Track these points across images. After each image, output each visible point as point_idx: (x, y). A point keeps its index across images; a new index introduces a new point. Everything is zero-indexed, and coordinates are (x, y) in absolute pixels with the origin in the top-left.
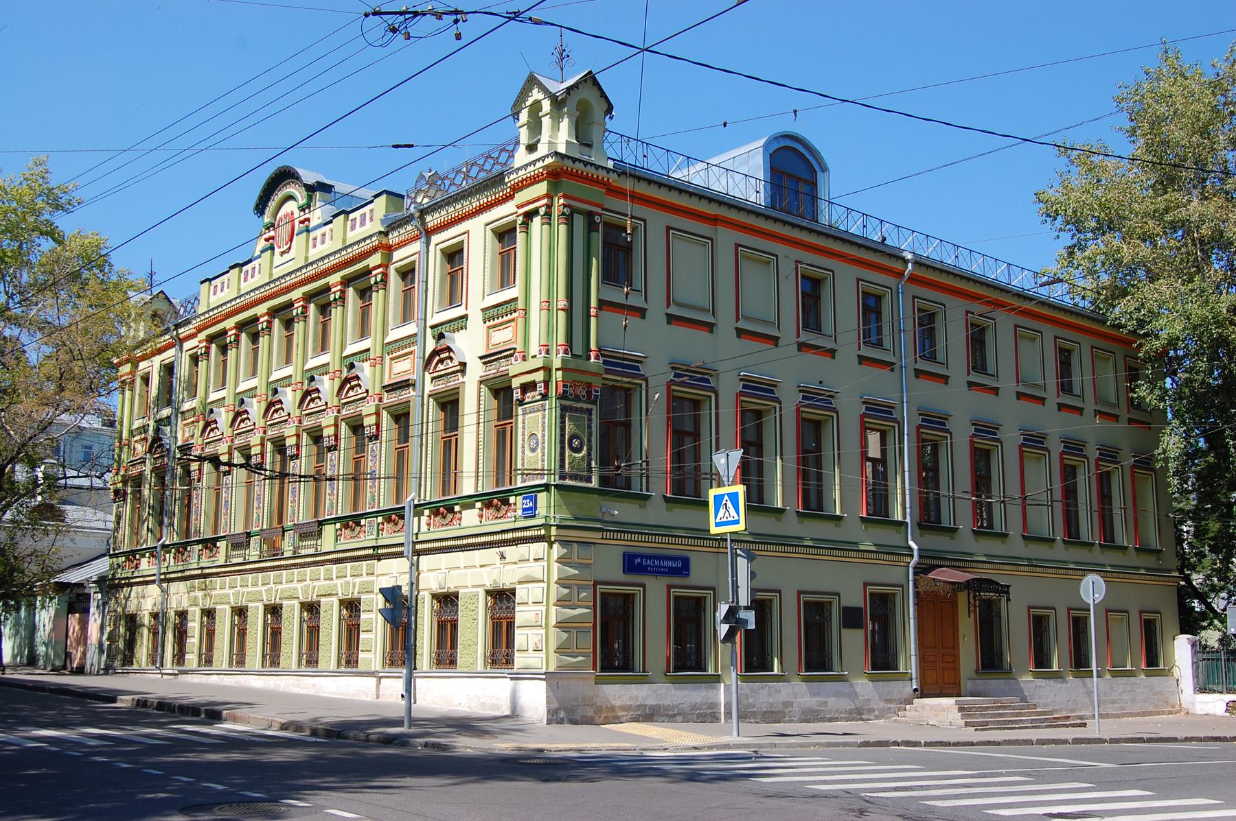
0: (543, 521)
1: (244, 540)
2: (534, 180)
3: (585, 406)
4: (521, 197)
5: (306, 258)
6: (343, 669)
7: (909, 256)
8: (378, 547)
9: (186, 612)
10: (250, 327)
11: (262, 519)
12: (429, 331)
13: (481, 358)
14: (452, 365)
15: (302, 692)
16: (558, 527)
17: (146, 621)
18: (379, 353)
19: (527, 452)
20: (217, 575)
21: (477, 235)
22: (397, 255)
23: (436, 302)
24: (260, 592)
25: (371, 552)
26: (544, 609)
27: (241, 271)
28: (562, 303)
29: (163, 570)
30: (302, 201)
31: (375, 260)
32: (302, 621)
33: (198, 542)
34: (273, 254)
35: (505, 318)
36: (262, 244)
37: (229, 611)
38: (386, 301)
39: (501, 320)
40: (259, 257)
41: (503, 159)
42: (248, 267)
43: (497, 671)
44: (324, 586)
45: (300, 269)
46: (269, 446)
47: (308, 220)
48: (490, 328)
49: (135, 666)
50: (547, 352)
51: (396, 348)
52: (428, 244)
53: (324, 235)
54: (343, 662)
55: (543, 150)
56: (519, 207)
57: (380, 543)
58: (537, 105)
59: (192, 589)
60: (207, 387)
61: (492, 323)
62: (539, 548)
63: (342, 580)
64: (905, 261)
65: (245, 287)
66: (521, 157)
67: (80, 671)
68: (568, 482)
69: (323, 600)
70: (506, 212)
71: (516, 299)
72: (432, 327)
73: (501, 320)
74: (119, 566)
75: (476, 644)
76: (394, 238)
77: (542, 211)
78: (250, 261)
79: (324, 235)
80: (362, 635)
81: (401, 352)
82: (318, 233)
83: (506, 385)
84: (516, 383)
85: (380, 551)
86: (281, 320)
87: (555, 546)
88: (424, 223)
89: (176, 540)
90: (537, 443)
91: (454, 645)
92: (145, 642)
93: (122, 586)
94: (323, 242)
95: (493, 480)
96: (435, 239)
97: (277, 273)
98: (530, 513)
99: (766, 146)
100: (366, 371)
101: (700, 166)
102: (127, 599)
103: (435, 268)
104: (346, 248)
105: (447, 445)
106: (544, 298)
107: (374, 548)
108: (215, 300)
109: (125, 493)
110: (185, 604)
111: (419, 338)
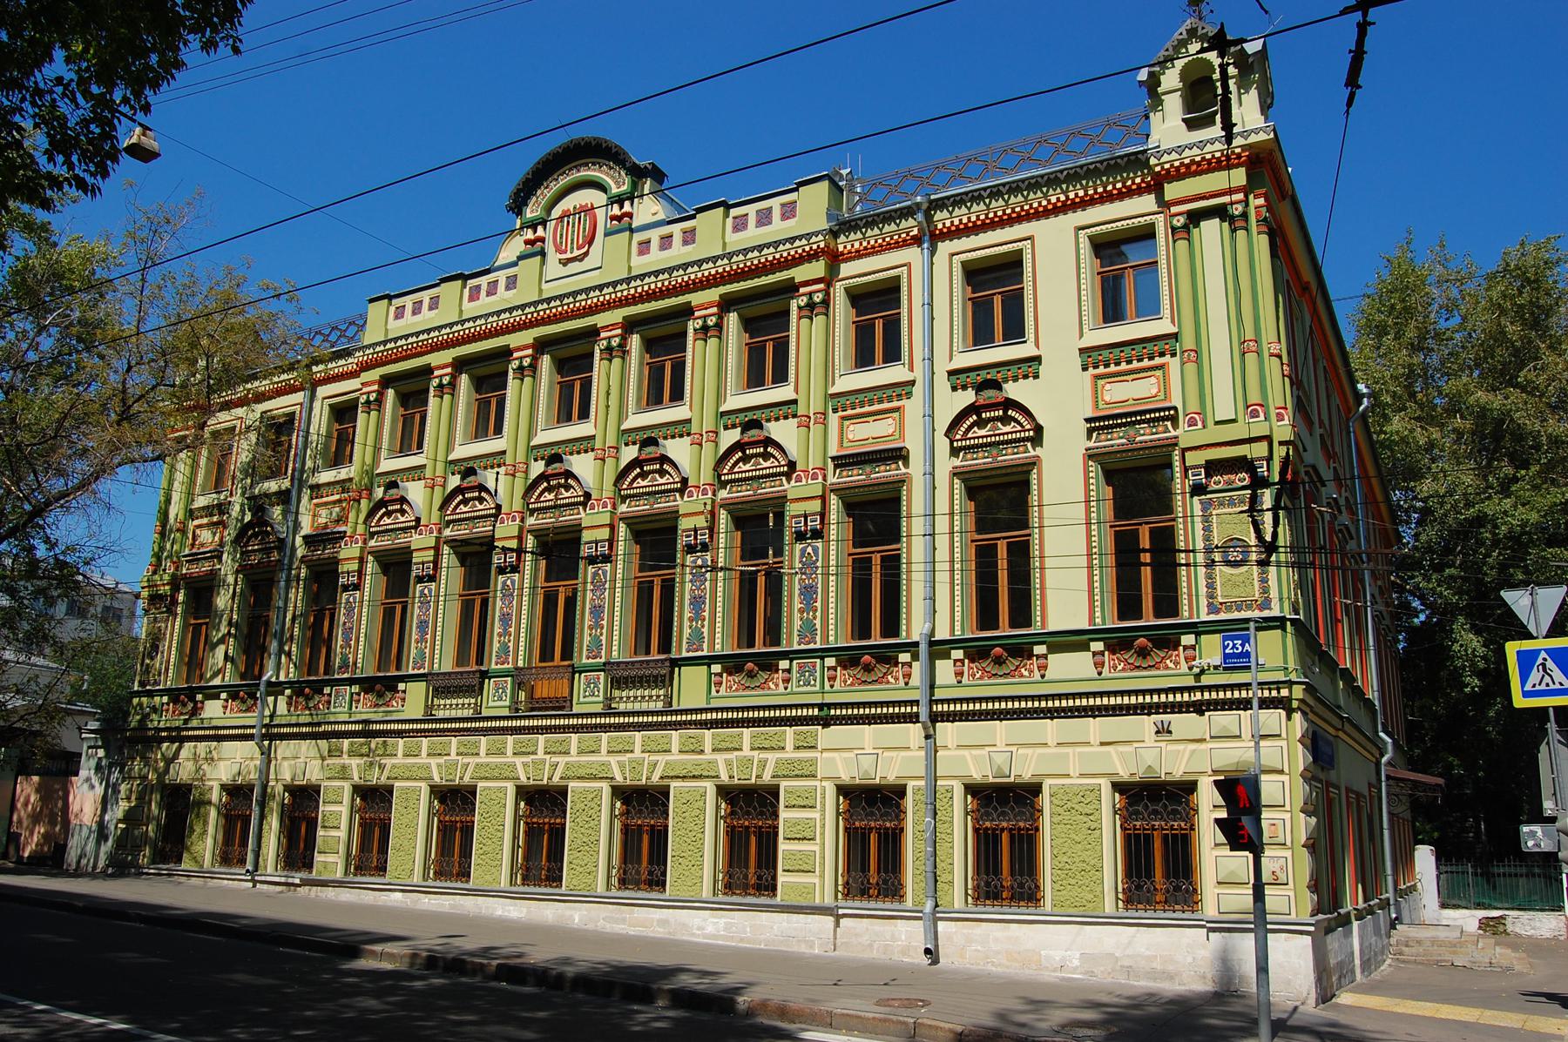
1: (476, 682)
6: (614, 892)
8: (830, 706)
9: (316, 789)
13: (1088, 420)
14: (487, 507)
15: (632, 931)
17: (215, 797)
20: (400, 734)
22: (846, 269)
24: (429, 767)
27: (726, 215)
29: (267, 721)
31: (817, 269)
33: (351, 682)
34: (543, 263)
36: (515, 247)
40: (515, 264)
41: (350, 333)
42: (483, 281)
44: (676, 761)
47: (630, 215)
49: (187, 864)
52: (933, 252)
54: (615, 881)
57: (829, 699)
59: (334, 752)
60: (377, 449)
62: (1272, 719)
67: (78, 873)
69: (674, 784)
74: (154, 709)
75: (1100, 870)
76: (843, 244)
78: (487, 272)
80: (320, 832)
82: (655, 235)
83: (892, 495)
86: (472, 378)
87: (1297, 716)
88: (929, 218)
89: (293, 675)
91: (383, 849)
92: (211, 829)
93: (163, 740)
95: (373, 662)
96: (322, 391)
97: (550, 290)
102: (170, 761)
105: (389, 614)
107: (821, 706)
108: (397, 327)
109: (174, 602)
111: (917, 390)
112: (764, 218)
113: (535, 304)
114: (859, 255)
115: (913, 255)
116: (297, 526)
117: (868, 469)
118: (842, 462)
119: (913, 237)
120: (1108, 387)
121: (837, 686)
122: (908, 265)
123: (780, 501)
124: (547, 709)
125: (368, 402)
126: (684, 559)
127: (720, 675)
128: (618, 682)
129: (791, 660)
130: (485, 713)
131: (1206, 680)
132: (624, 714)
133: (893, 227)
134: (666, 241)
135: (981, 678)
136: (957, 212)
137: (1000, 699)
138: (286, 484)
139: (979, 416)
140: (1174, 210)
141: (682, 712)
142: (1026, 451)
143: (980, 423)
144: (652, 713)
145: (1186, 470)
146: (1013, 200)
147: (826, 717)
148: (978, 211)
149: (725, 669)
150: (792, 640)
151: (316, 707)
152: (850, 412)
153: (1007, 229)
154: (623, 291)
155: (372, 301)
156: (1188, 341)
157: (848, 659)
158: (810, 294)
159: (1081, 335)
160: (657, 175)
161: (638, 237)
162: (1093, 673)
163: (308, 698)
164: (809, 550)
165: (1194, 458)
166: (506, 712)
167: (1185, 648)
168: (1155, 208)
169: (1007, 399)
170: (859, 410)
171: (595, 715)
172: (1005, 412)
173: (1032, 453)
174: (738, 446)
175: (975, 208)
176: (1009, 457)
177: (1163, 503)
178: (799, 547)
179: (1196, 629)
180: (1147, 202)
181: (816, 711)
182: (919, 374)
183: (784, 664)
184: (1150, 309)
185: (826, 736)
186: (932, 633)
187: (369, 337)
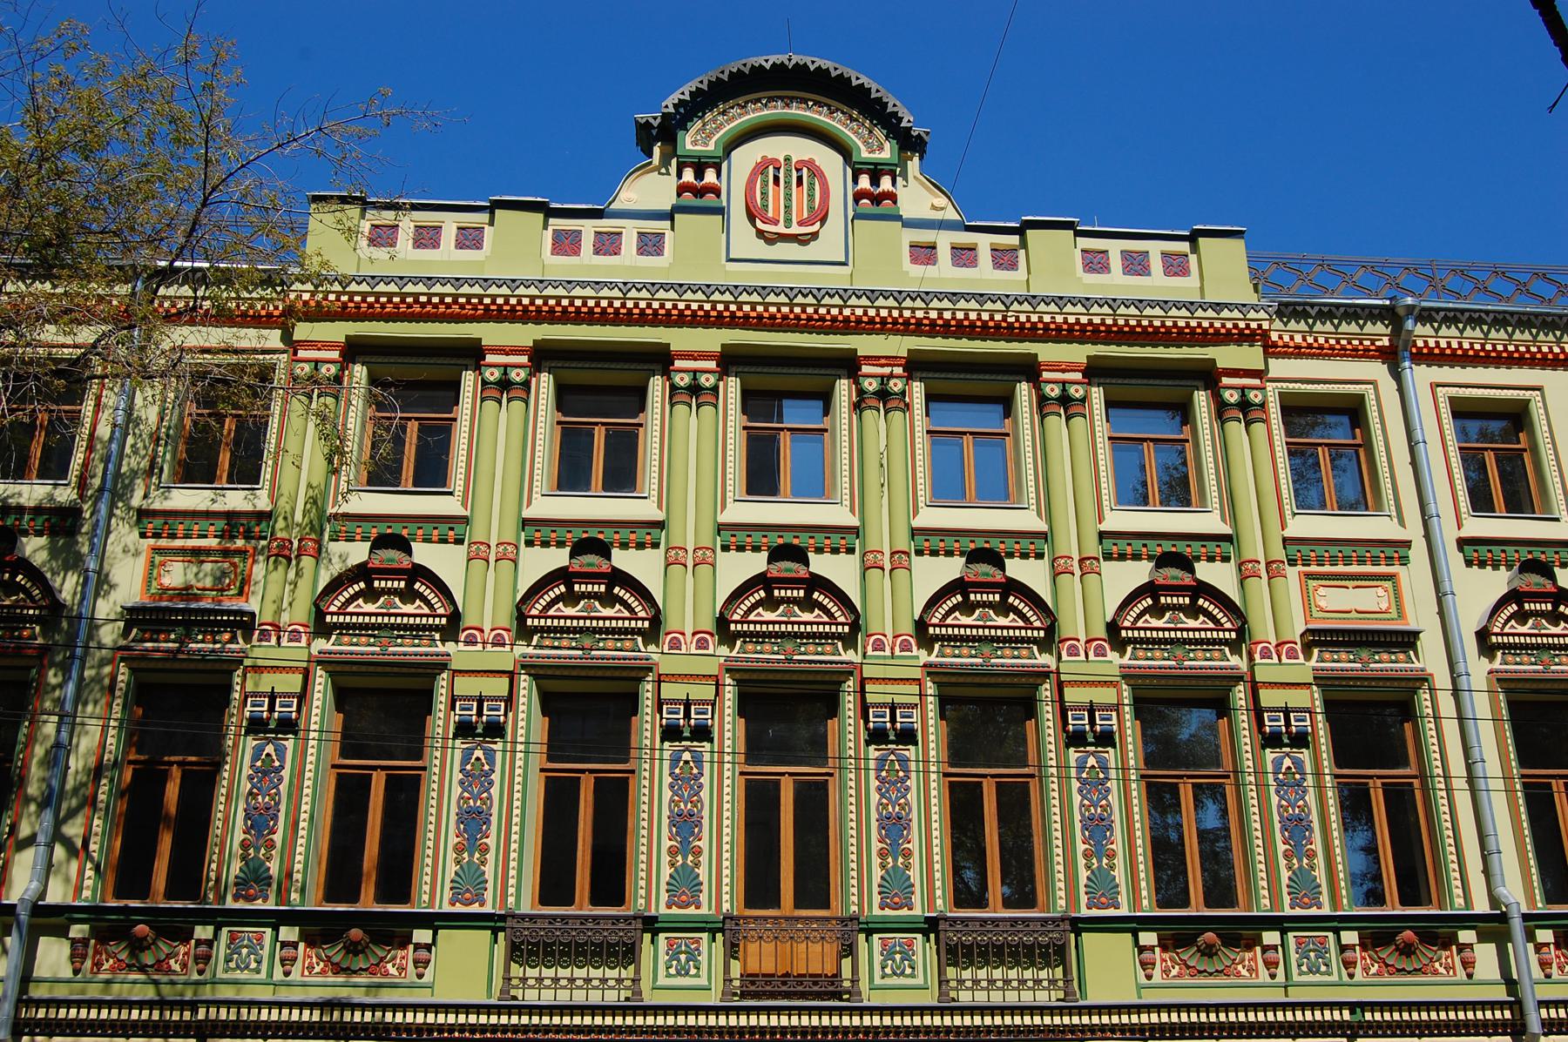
107: (1353, 1006)
111: (1418, 553)
112: (427, 238)
113: (1189, 306)
114: (1298, 352)
116: (101, 583)
117: (1365, 654)
118: (1317, 639)
119: (1379, 349)
120: (1322, 591)
121: (296, 975)
122: (1435, 386)
123: (638, 673)
124: (773, 995)
126: (866, 752)
127: (295, 945)
128: (954, 954)
129: (1284, 932)
130: (650, 998)
132: (972, 1010)
133: (1353, 328)
135: (1179, 976)
136: (1444, 331)
137: (1227, 1007)
138: (65, 495)
139: (966, 596)
140: (302, 354)
141: (1100, 1009)
142: (1033, 657)
143: (571, 598)
144: (1041, 1010)
145: (453, 700)
146: (1518, 335)
148: (1472, 337)
149: (304, 937)
151: (160, 966)
152: (1314, 568)
153: (1503, 370)
155: (316, 199)
157: (318, 929)
158: (317, 363)
159: (916, 513)
162: (66, 972)
163: (137, 946)
164: (270, 749)
165: (465, 686)
166: (713, 999)
167: (418, 947)
168: (281, 346)
169: (615, 570)
170: (1327, 569)
171: (922, 1010)
172: (610, 588)
173: (440, 648)
174: (362, 572)
175: (1468, 332)
176: (608, 652)
177: (620, 745)
178: (251, 742)
179: (433, 921)
180: (273, 338)
181: (1346, 1015)
183: (203, 932)
184: (817, 488)
186: (43, 895)
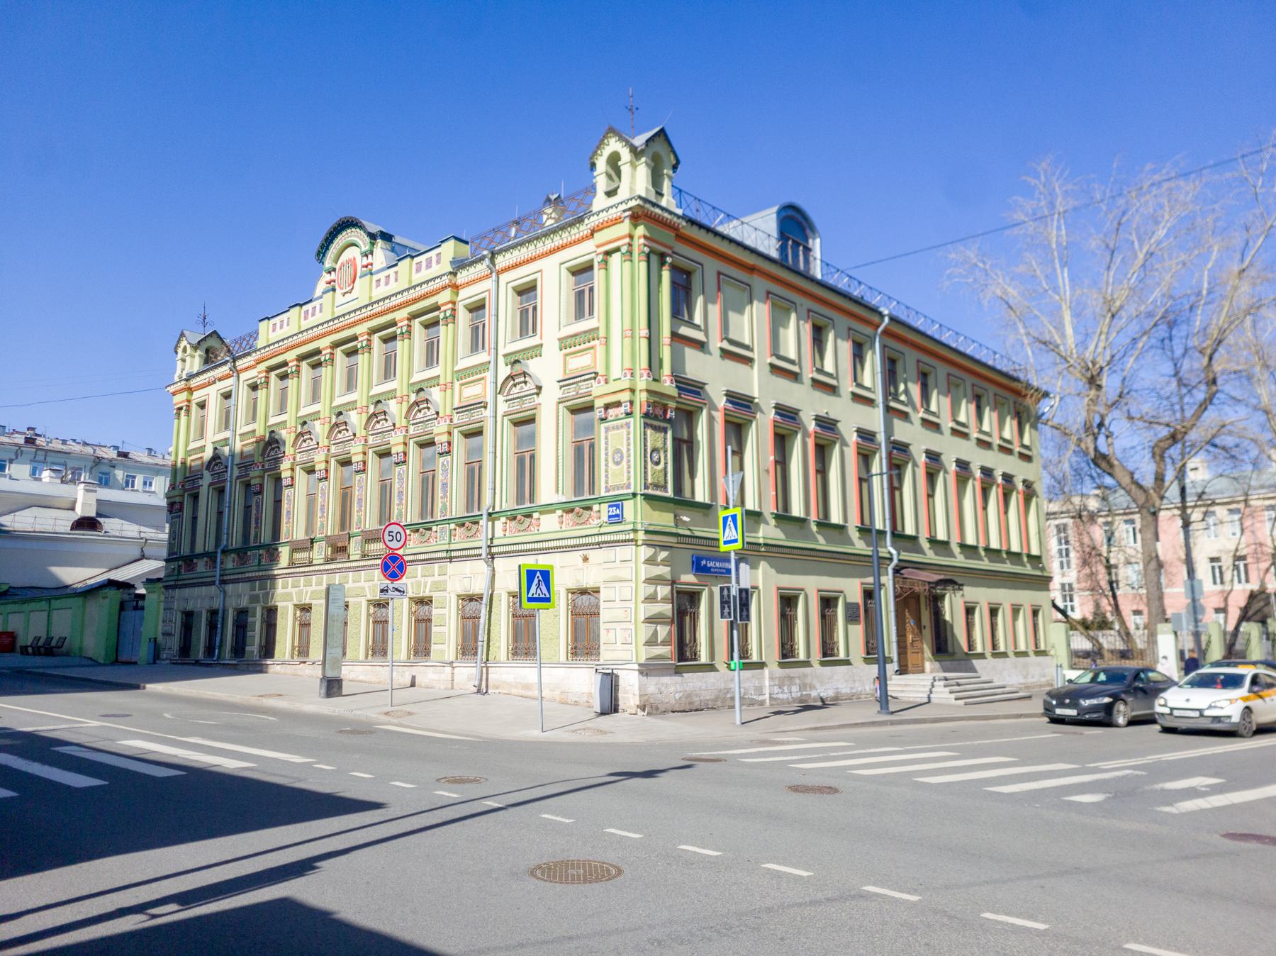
0: (631, 527)
2: (618, 221)
3: (662, 424)
4: (600, 237)
5: (410, 281)
7: (886, 312)
10: (313, 359)
11: (328, 525)
12: (501, 360)
16: (647, 532)
18: (449, 380)
19: (611, 464)
21: (552, 276)
22: (463, 293)
23: (509, 334)
24: (363, 588)
25: (444, 555)
26: (633, 606)
28: (645, 332)
30: (365, 247)
31: (445, 296)
32: (369, 615)
35: (583, 346)
37: (364, 604)
38: (454, 336)
39: (578, 348)
40: (321, 297)
42: (309, 307)
43: (581, 661)
45: (366, 306)
46: (333, 461)
48: (566, 355)
50: (632, 375)
51: (465, 375)
53: (388, 277)
55: (623, 193)
56: (598, 246)
57: (453, 547)
58: (614, 160)
61: (568, 350)
62: (626, 552)
63: (371, 583)
64: (881, 315)
65: (305, 324)
66: (600, 201)
68: (650, 491)
70: (586, 251)
71: (597, 329)
72: (505, 356)
73: (578, 348)
75: (558, 638)
76: (463, 277)
77: (624, 249)
79: (388, 277)
80: (434, 629)
81: (472, 378)
82: (382, 276)
84: (599, 403)
85: (453, 554)
90: (622, 457)
94: (387, 284)
96: (504, 278)
98: (617, 519)
99: (779, 213)
100: (435, 394)
101: (735, 222)
103: (506, 307)
104: (372, 304)
106: (627, 325)
108: (274, 337)
110: (244, 603)
111: (492, 366)
115: (489, 284)
125: (446, 318)
131: (603, 530)
134: (429, 262)
147: (449, 557)
150: (438, 516)
154: (366, 313)
156: (602, 333)
160: (387, 237)
161: (375, 277)
182: (492, 358)
185: (452, 568)
187: (260, 343)
